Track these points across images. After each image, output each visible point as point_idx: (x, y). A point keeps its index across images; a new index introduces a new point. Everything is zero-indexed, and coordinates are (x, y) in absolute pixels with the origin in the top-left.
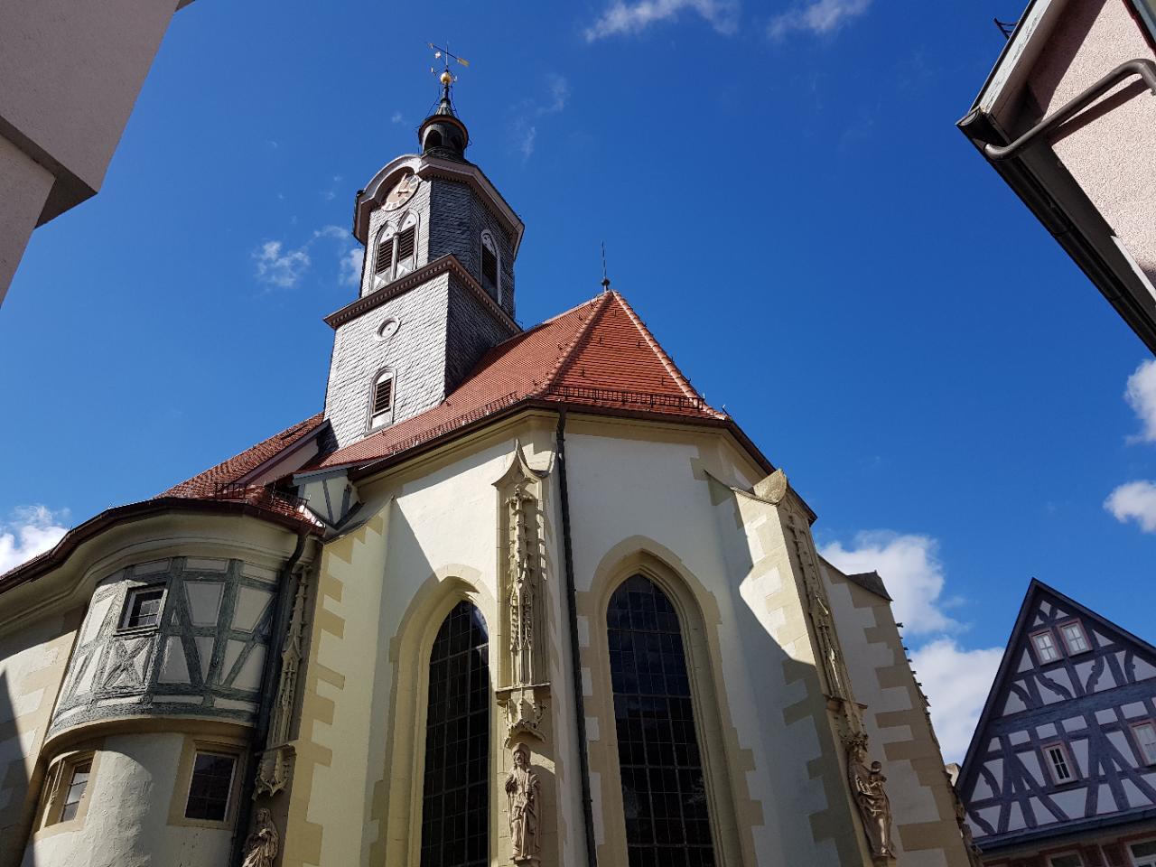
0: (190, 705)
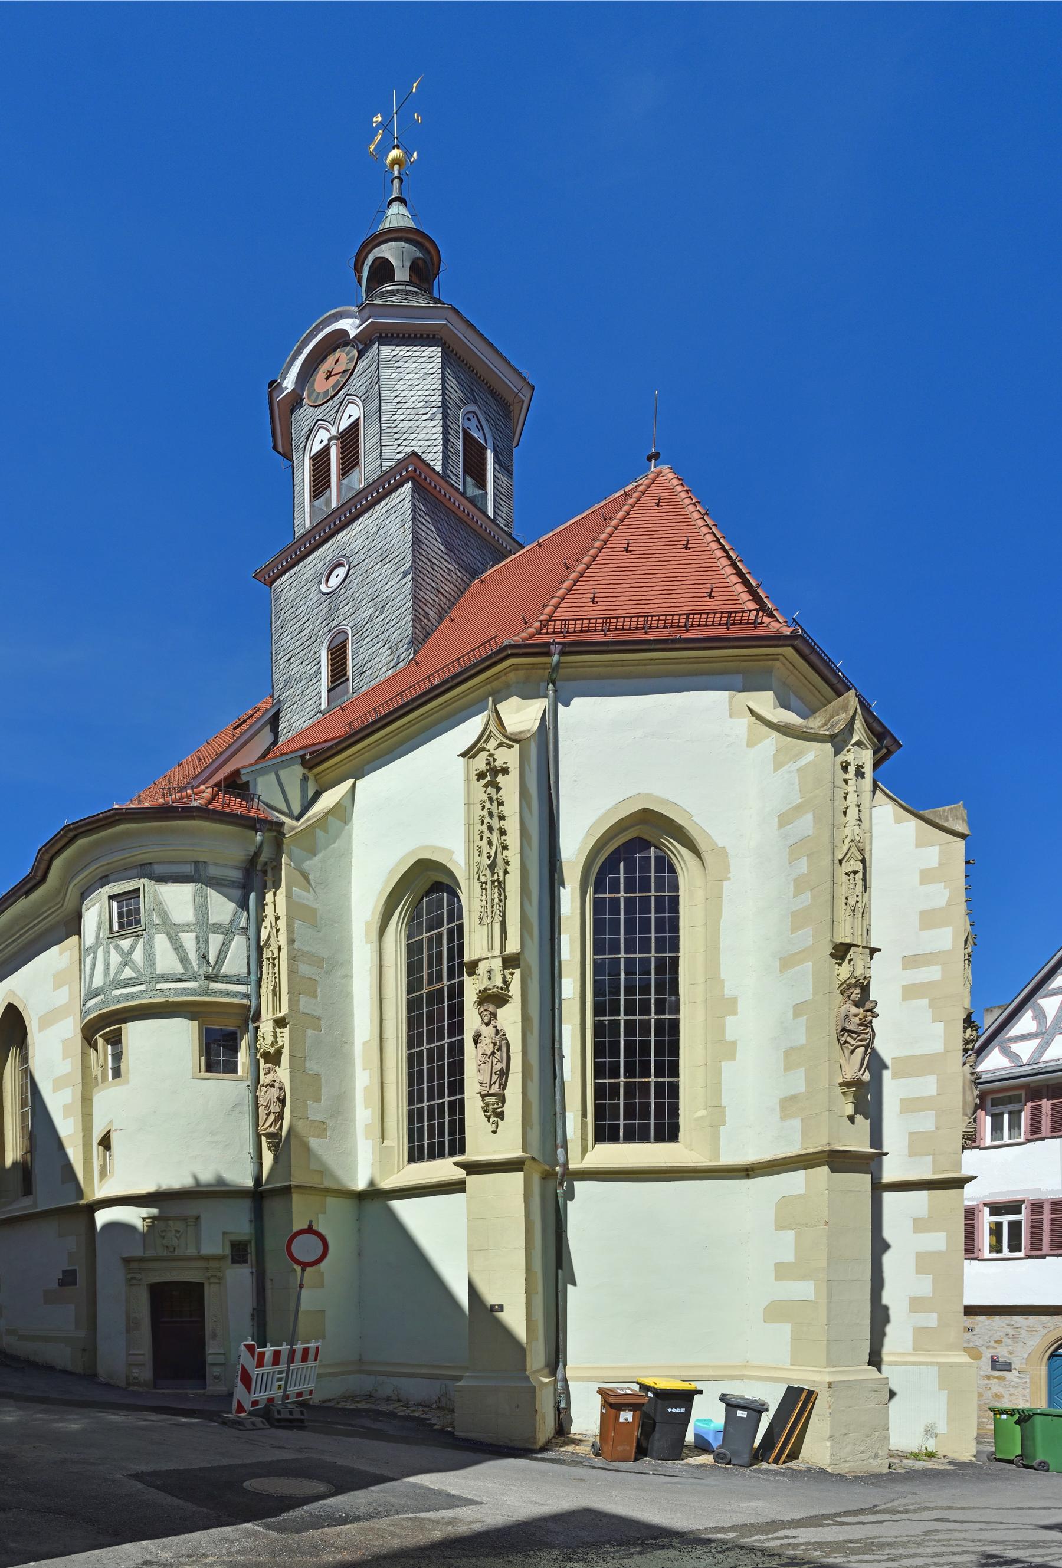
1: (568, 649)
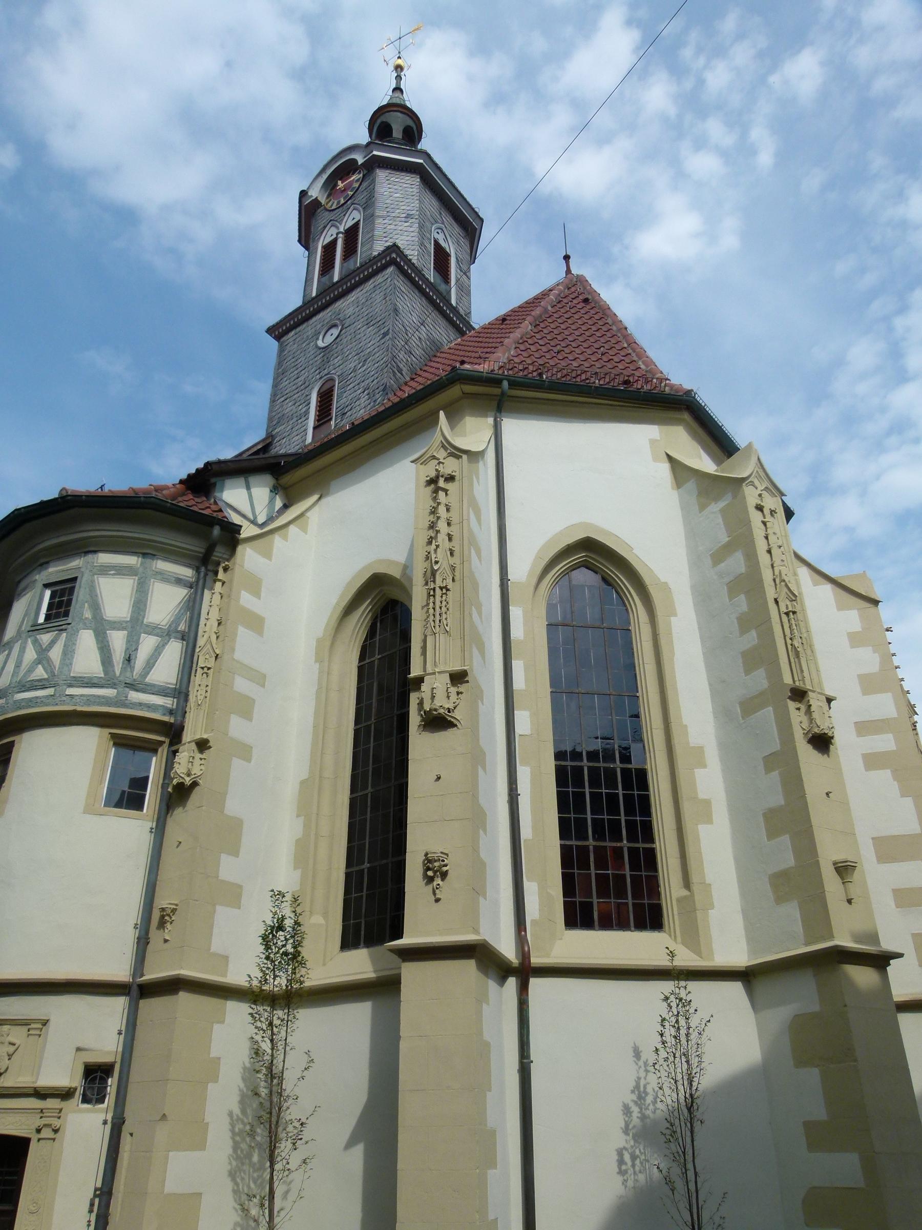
0: (103, 697)
1: (513, 384)
